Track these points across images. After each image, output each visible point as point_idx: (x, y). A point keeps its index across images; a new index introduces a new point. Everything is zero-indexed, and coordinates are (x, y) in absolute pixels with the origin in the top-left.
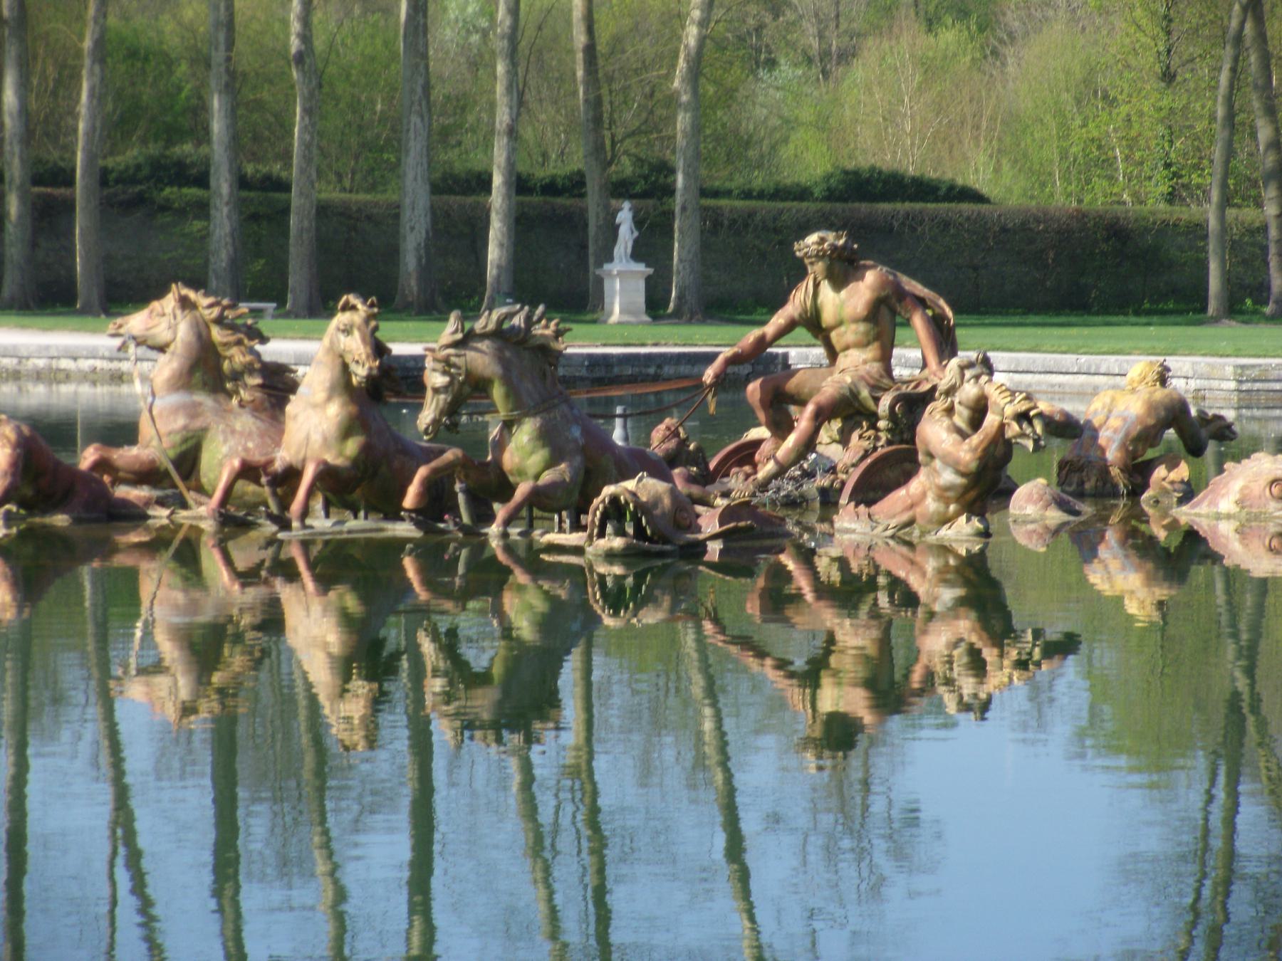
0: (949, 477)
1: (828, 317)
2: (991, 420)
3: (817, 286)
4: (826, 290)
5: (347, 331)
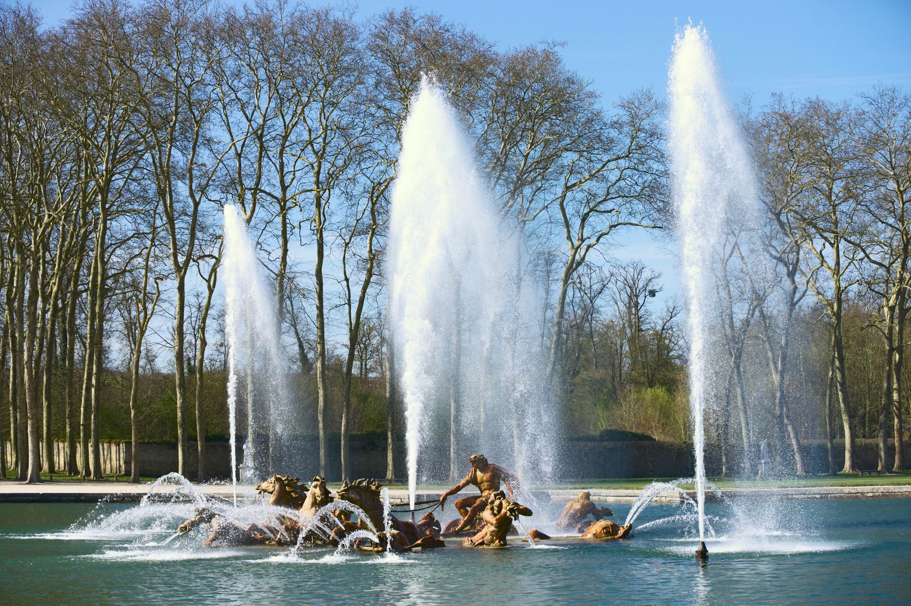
0: (492, 528)
1: (479, 480)
2: (503, 511)
3: (475, 471)
4: (479, 473)
5: (315, 487)
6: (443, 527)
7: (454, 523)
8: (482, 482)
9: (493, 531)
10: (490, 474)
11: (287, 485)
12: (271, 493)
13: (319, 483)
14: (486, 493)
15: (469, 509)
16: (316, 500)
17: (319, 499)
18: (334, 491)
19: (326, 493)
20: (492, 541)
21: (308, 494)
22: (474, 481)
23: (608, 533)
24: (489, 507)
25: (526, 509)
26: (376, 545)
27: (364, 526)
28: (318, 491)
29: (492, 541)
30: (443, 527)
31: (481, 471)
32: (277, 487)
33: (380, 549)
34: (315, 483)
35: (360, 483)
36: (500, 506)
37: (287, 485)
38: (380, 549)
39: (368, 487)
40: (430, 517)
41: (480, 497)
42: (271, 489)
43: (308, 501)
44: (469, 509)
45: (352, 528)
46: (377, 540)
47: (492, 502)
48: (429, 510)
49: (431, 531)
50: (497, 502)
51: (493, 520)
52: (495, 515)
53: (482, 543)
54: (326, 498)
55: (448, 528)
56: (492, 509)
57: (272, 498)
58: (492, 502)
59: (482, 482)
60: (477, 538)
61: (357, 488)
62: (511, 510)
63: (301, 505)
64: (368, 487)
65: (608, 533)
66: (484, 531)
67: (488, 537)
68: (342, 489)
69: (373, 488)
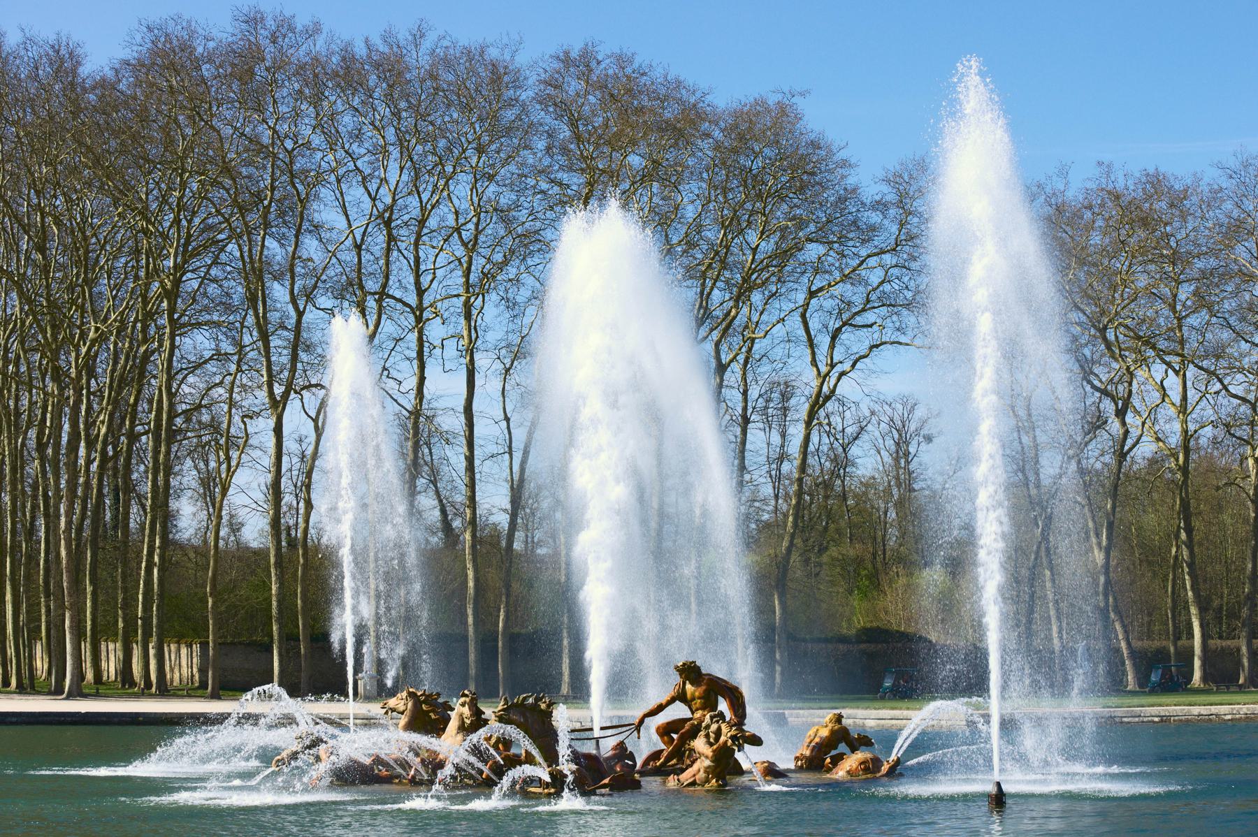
0: (707, 763)
1: (689, 696)
2: (723, 739)
3: (684, 684)
5: (463, 705)
6: (639, 763)
7: (656, 755)
8: (693, 699)
9: (709, 767)
10: (704, 687)
11: (424, 702)
12: (402, 713)
13: (468, 700)
14: (698, 714)
15: (675, 736)
16: (463, 722)
17: (468, 722)
18: (489, 712)
19: (477, 713)
20: (707, 781)
21: (453, 715)
22: (681, 697)
23: (866, 770)
24: (702, 733)
25: (754, 736)
26: (548, 785)
27: (530, 760)
28: (466, 711)
29: (707, 781)
30: (639, 763)
31: (692, 684)
32: (410, 705)
33: (552, 790)
34: (463, 699)
35: (525, 699)
36: (718, 733)
37: (424, 702)
38: (552, 790)
39: (535, 706)
40: (621, 746)
41: (691, 719)
42: (402, 708)
43: (453, 725)
44: (675, 736)
45: (514, 761)
46: (547, 779)
47: (708, 727)
48: (621, 738)
49: (622, 767)
50: (714, 727)
51: (708, 751)
52: (711, 745)
53: (693, 784)
54: (478, 721)
55: (646, 762)
56: (707, 736)
57: (403, 720)
58: (708, 727)
59: (693, 699)
60: (686, 776)
61: (521, 706)
62: (734, 738)
63: (444, 730)
64: (535, 706)
65: (866, 770)
66: (696, 767)
67: (702, 775)
68: (500, 708)
69: (543, 706)
